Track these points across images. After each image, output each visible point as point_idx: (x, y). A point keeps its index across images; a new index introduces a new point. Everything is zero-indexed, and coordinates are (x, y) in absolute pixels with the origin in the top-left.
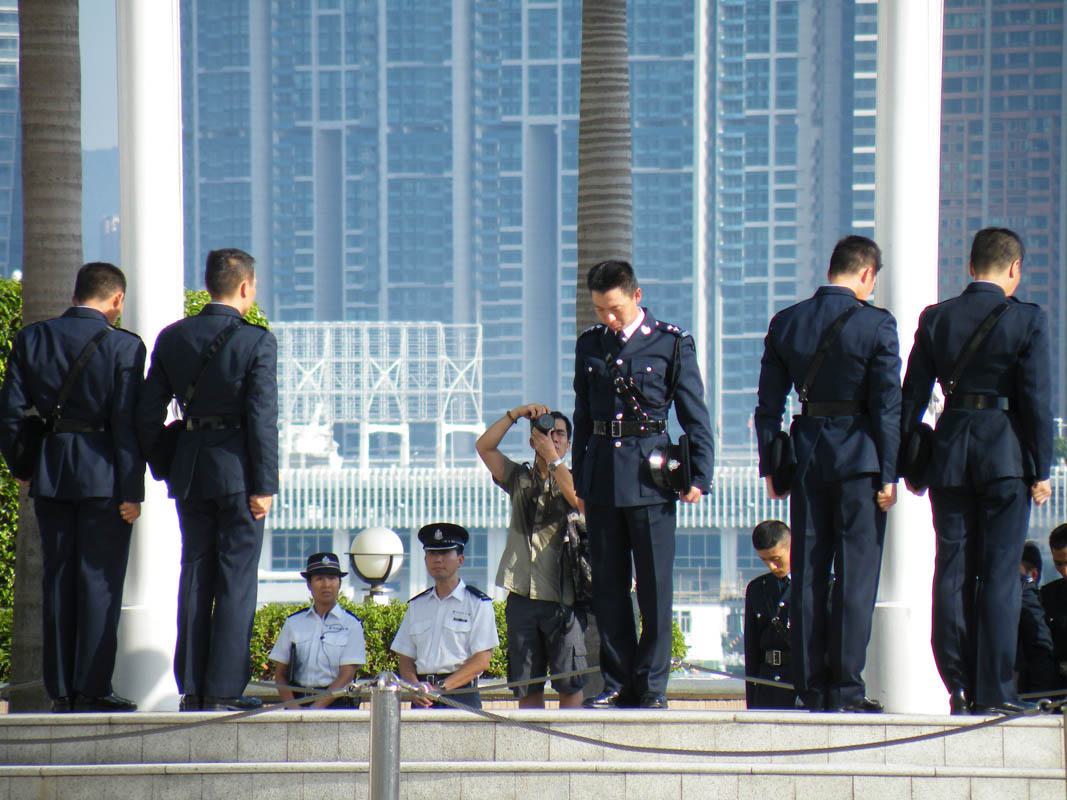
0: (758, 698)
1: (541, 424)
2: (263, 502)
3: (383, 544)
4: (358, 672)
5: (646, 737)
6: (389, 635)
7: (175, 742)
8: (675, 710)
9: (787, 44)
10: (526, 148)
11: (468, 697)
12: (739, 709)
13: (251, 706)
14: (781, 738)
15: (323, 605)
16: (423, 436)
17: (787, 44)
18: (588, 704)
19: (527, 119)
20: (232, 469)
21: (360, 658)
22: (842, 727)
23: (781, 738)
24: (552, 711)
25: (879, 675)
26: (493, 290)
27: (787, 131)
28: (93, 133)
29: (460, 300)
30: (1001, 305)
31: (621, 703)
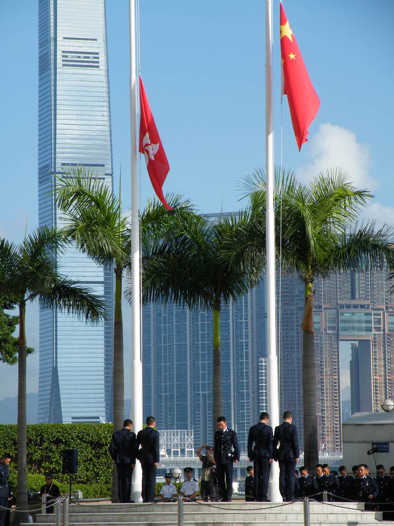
0: (248, 499)
1: (208, 448)
2: (156, 464)
3: (178, 471)
4: (175, 495)
5: (228, 507)
6: (179, 489)
7: (142, 508)
8: (233, 502)
9: (247, 379)
10: (201, 398)
11: (195, 500)
12: (244, 502)
13: (156, 502)
14: (252, 507)
15: (168, 483)
16: (183, 451)
17: (247, 379)
18: (217, 501)
19: (201, 392)
20: (151, 457)
21: (176, 493)
22: (264, 505)
23: (252, 507)
24: (209, 502)
25: (270, 496)
26: (195, 423)
27: (248, 395)
28: (126, 397)
29: (189, 426)
30: (152, 430)
31: (223, 501)
